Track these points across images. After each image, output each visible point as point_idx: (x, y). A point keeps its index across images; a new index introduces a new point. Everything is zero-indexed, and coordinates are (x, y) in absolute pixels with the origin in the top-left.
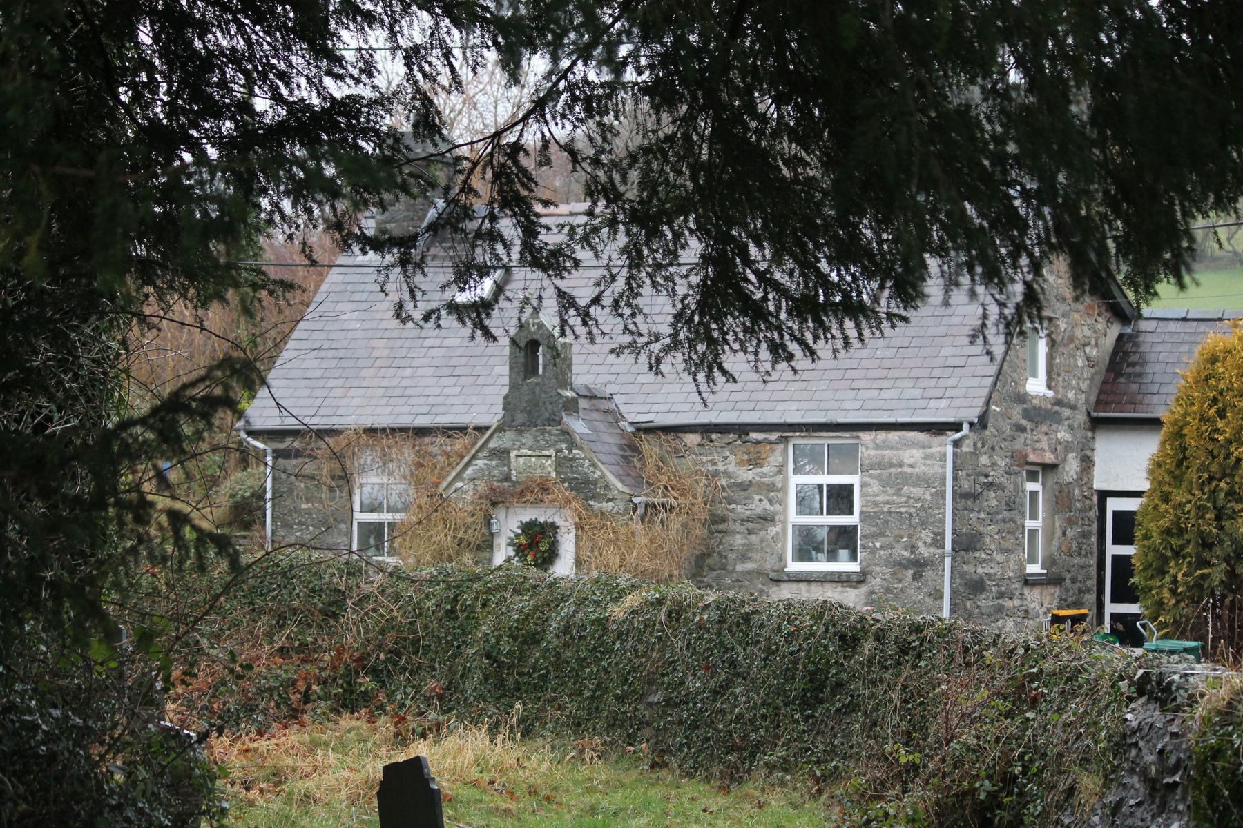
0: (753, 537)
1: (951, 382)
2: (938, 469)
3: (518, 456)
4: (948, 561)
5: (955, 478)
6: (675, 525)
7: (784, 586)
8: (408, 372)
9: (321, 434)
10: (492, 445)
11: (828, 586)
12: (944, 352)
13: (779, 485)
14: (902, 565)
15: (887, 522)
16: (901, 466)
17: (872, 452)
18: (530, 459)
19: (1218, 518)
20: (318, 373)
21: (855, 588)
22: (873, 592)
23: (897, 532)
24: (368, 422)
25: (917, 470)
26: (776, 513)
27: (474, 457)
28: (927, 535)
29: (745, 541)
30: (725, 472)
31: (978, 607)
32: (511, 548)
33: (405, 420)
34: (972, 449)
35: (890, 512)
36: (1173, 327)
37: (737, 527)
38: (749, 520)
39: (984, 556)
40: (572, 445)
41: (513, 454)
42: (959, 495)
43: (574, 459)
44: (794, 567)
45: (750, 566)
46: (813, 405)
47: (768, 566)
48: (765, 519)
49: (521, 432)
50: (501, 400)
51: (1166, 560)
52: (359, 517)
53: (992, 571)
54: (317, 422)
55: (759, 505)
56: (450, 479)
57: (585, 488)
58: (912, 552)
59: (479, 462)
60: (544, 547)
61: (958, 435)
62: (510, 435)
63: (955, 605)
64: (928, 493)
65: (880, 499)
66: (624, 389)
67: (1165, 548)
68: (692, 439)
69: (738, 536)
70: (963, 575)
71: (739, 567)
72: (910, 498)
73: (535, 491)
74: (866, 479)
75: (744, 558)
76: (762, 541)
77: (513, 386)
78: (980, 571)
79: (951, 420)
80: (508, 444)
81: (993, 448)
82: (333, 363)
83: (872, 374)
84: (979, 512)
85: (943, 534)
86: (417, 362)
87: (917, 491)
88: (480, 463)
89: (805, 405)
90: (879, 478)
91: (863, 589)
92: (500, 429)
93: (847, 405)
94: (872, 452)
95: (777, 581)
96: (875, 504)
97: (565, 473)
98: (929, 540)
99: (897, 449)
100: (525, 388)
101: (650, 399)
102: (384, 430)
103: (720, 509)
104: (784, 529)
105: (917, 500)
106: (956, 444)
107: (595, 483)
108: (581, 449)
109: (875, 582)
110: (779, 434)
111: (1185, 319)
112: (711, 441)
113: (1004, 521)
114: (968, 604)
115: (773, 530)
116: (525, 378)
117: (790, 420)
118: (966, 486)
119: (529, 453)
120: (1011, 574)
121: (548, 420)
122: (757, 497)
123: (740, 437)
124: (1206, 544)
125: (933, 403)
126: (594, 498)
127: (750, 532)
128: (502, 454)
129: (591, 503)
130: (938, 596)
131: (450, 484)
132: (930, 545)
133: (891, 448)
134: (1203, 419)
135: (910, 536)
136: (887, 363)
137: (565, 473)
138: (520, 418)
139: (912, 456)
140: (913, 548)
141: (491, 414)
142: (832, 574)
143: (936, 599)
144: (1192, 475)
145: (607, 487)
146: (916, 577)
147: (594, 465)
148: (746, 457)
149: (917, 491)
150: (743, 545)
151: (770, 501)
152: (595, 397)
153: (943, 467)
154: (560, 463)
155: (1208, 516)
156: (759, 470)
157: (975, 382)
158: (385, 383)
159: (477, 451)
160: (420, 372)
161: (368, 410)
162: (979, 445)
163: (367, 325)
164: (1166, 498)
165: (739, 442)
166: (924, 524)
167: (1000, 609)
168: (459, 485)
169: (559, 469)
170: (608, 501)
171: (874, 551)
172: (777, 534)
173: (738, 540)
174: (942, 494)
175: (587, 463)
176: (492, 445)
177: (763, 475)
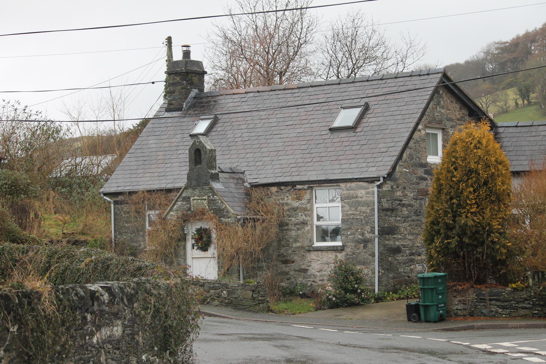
0: (299, 231)
1: (380, 159)
2: (371, 198)
3: (193, 200)
4: (377, 239)
5: (379, 202)
6: (259, 228)
7: (312, 253)
8: (169, 165)
9: (131, 193)
10: (184, 195)
11: (329, 252)
12: (380, 146)
13: (309, 208)
14: (358, 242)
15: (352, 223)
16: (357, 198)
17: (345, 192)
18: (198, 201)
19: (454, 216)
20: (135, 167)
21: (340, 253)
22: (347, 255)
23: (356, 227)
24: (148, 187)
25: (363, 199)
26: (308, 221)
27: (177, 201)
28: (368, 228)
29: (296, 234)
30: (287, 204)
31: (397, 260)
32: (193, 240)
33: (163, 186)
34: (390, 189)
35: (353, 218)
36: (511, 130)
37: (293, 228)
38: (297, 224)
39: (400, 237)
40: (214, 194)
41: (191, 199)
42: (382, 210)
43: (215, 200)
44: (317, 244)
45: (298, 244)
46: (322, 172)
47: (305, 244)
48: (304, 224)
49: (194, 189)
50: (186, 176)
51: (433, 236)
52: (316, 223)
53: (406, 243)
54: (128, 188)
55: (301, 217)
56: (168, 211)
57: (219, 213)
58: (363, 236)
59: (179, 203)
60: (205, 239)
61: (378, 183)
62: (190, 190)
63: (381, 259)
64: (368, 209)
65: (349, 213)
66: (250, 168)
67: (432, 231)
68: (274, 189)
69: (293, 231)
70: (384, 246)
71: (294, 245)
72: (361, 212)
73: (200, 215)
74: (343, 204)
75: (296, 241)
76: (303, 233)
77: (191, 169)
78: (397, 243)
79: (375, 176)
80: (190, 195)
81: (404, 188)
82: (141, 163)
83: (349, 157)
84: (396, 217)
85: (374, 228)
86: (173, 161)
87: (364, 209)
88: (179, 203)
89: (319, 172)
90: (348, 203)
91: (344, 253)
92: (186, 188)
93: (335, 171)
94: (345, 192)
95: (309, 251)
96: (347, 215)
97: (212, 207)
98: (369, 230)
99: (355, 190)
100: (195, 170)
101: (259, 172)
102: (154, 191)
103: (286, 220)
104: (312, 227)
105: (364, 212)
106: (379, 187)
107: (223, 210)
108: (217, 195)
109: (348, 250)
110: (308, 186)
111: (516, 126)
112: (282, 190)
113: (413, 221)
114: (390, 259)
115: (307, 228)
116: (195, 166)
117: (311, 179)
118: (386, 205)
119: (198, 198)
120: (419, 245)
121: (204, 183)
122: (300, 214)
123: (293, 187)
124: (449, 228)
125: (371, 169)
126: (224, 216)
127: (298, 229)
128: (187, 199)
129: (222, 219)
130: (373, 255)
131: (168, 213)
132: (370, 233)
133: (353, 190)
134: (449, 171)
135: (362, 229)
136: (356, 152)
137: (212, 207)
138: (194, 183)
139: (361, 193)
140: (363, 234)
141: (182, 183)
142: (330, 247)
143: (373, 257)
144: (443, 197)
145: (228, 212)
146: (365, 247)
147: (222, 202)
148: (295, 196)
149: (364, 209)
150: (296, 235)
151: (305, 215)
152: (234, 173)
153: (374, 197)
154: (210, 202)
155: (449, 215)
156: (301, 202)
157: (389, 159)
158: (159, 170)
159: (178, 198)
160: (174, 165)
161: (150, 182)
162: (395, 187)
163: (159, 145)
164: (432, 208)
165: (293, 190)
166: (367, 223)
167: (412, 261)
168: (172, 213)
169: (209, 205)
170: (229, 218)
171: (347, 236)
172: (309, 230)
173: (293, 233)
174: (373, 210)
175: (220, 202)
176: (184, 195)
177: (302, 204)
